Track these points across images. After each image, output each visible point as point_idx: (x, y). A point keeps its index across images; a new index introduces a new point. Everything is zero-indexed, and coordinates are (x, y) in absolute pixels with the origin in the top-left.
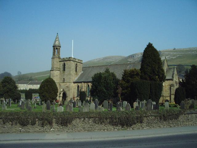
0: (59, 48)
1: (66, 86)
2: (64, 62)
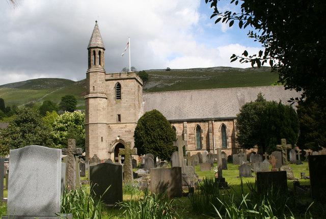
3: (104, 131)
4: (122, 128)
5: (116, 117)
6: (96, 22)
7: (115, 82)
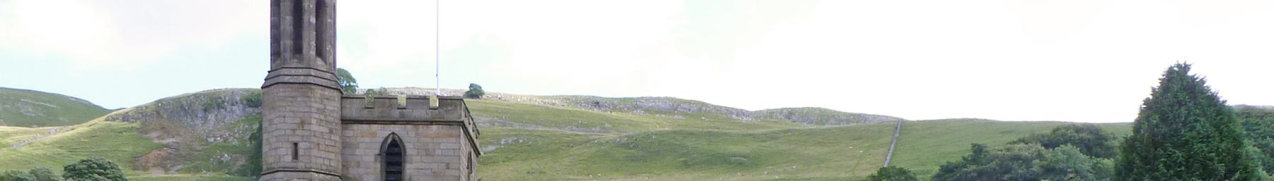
2: (397, 129)
7: (382, 132)
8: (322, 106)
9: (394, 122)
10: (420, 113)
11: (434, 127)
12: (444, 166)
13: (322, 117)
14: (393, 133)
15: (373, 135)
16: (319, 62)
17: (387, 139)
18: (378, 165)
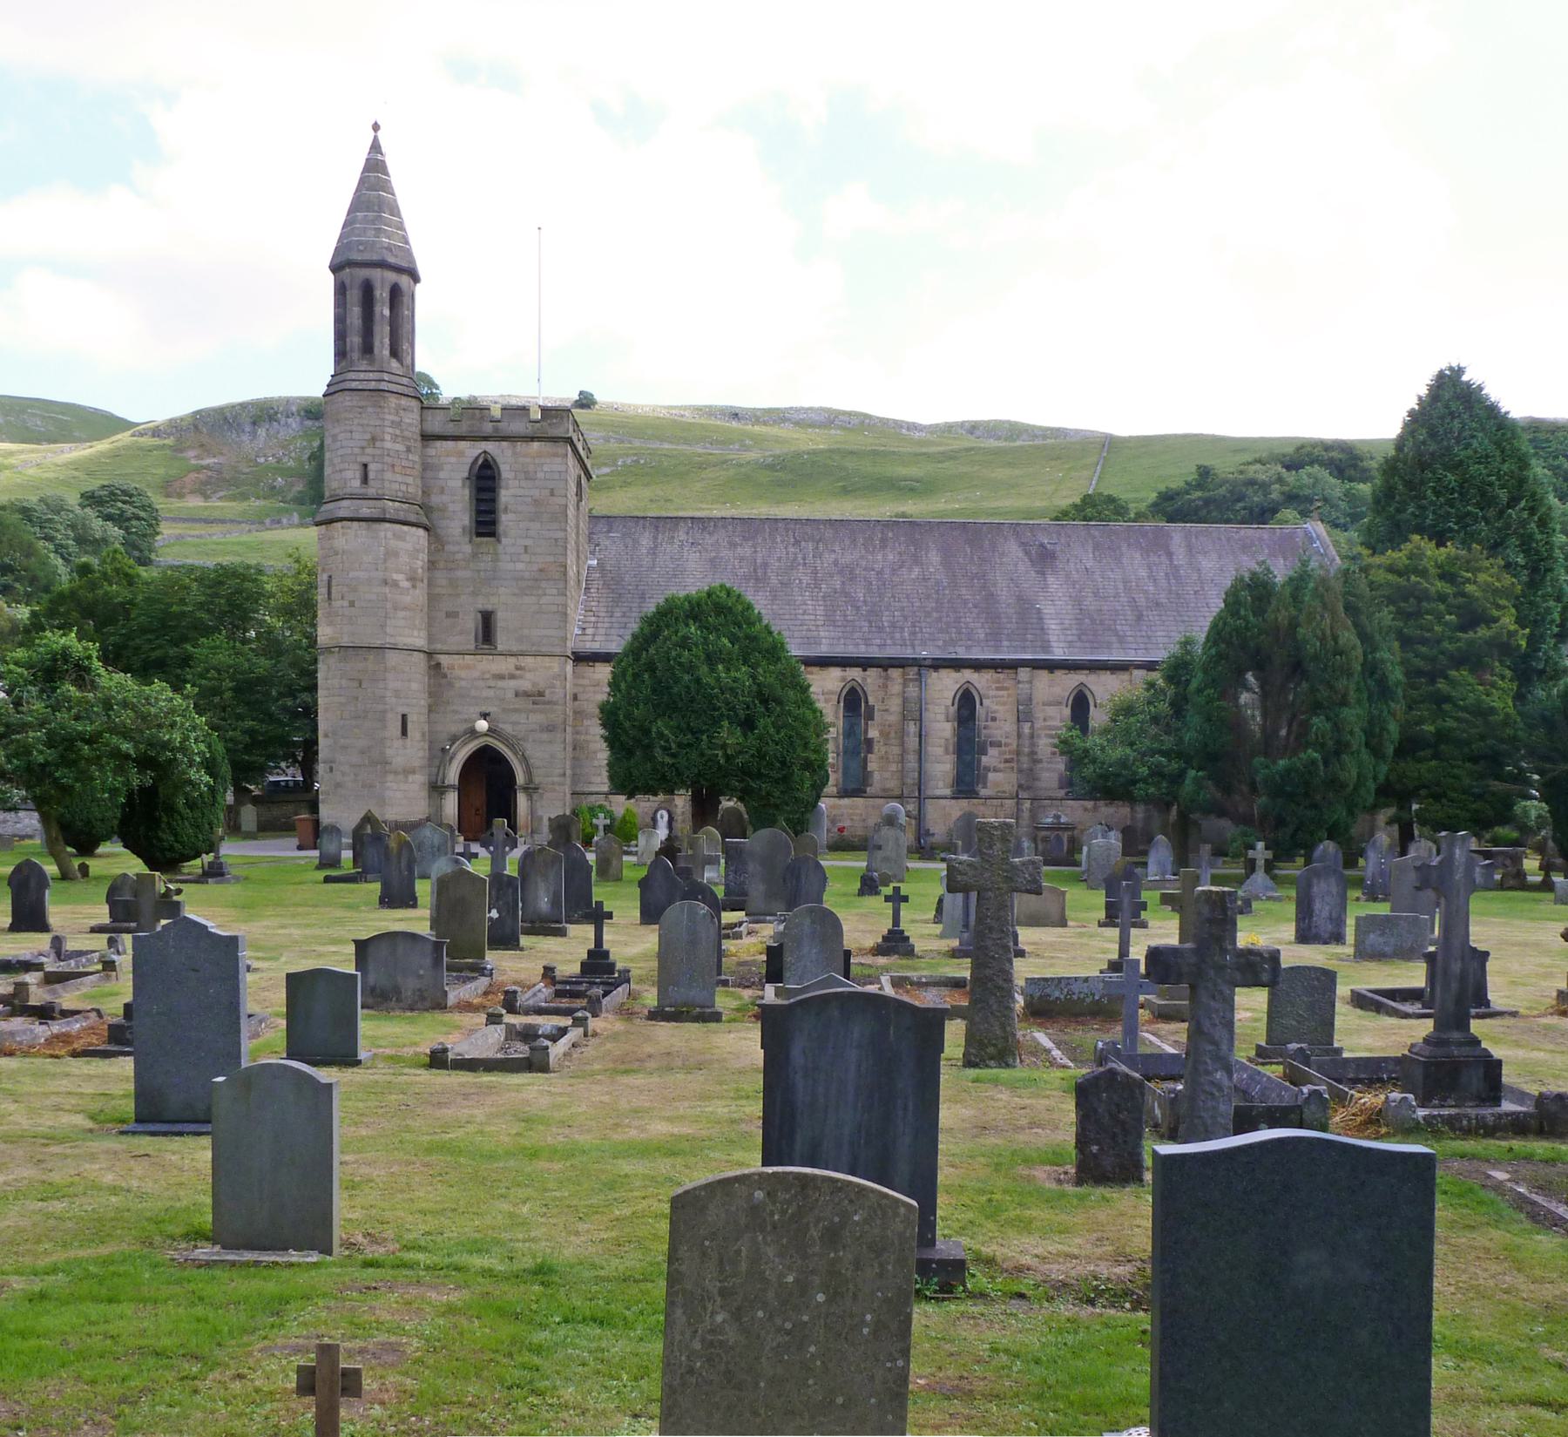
0: (396, 294)
1: (525, 684)
2: (490, 447)
3: (414, 686)
4: (501, 677)
5: (471, 622)
6: (376, 127)
8: (397, 419)
9: (486, 439)
10: (518, 427)
11: (536, 445)
12: (547, 492)
13: (398, 432)
14: (485, 452)
15: (461, 454)
16: (394, 364)
17: (477, 459)
18: (467, 492)
